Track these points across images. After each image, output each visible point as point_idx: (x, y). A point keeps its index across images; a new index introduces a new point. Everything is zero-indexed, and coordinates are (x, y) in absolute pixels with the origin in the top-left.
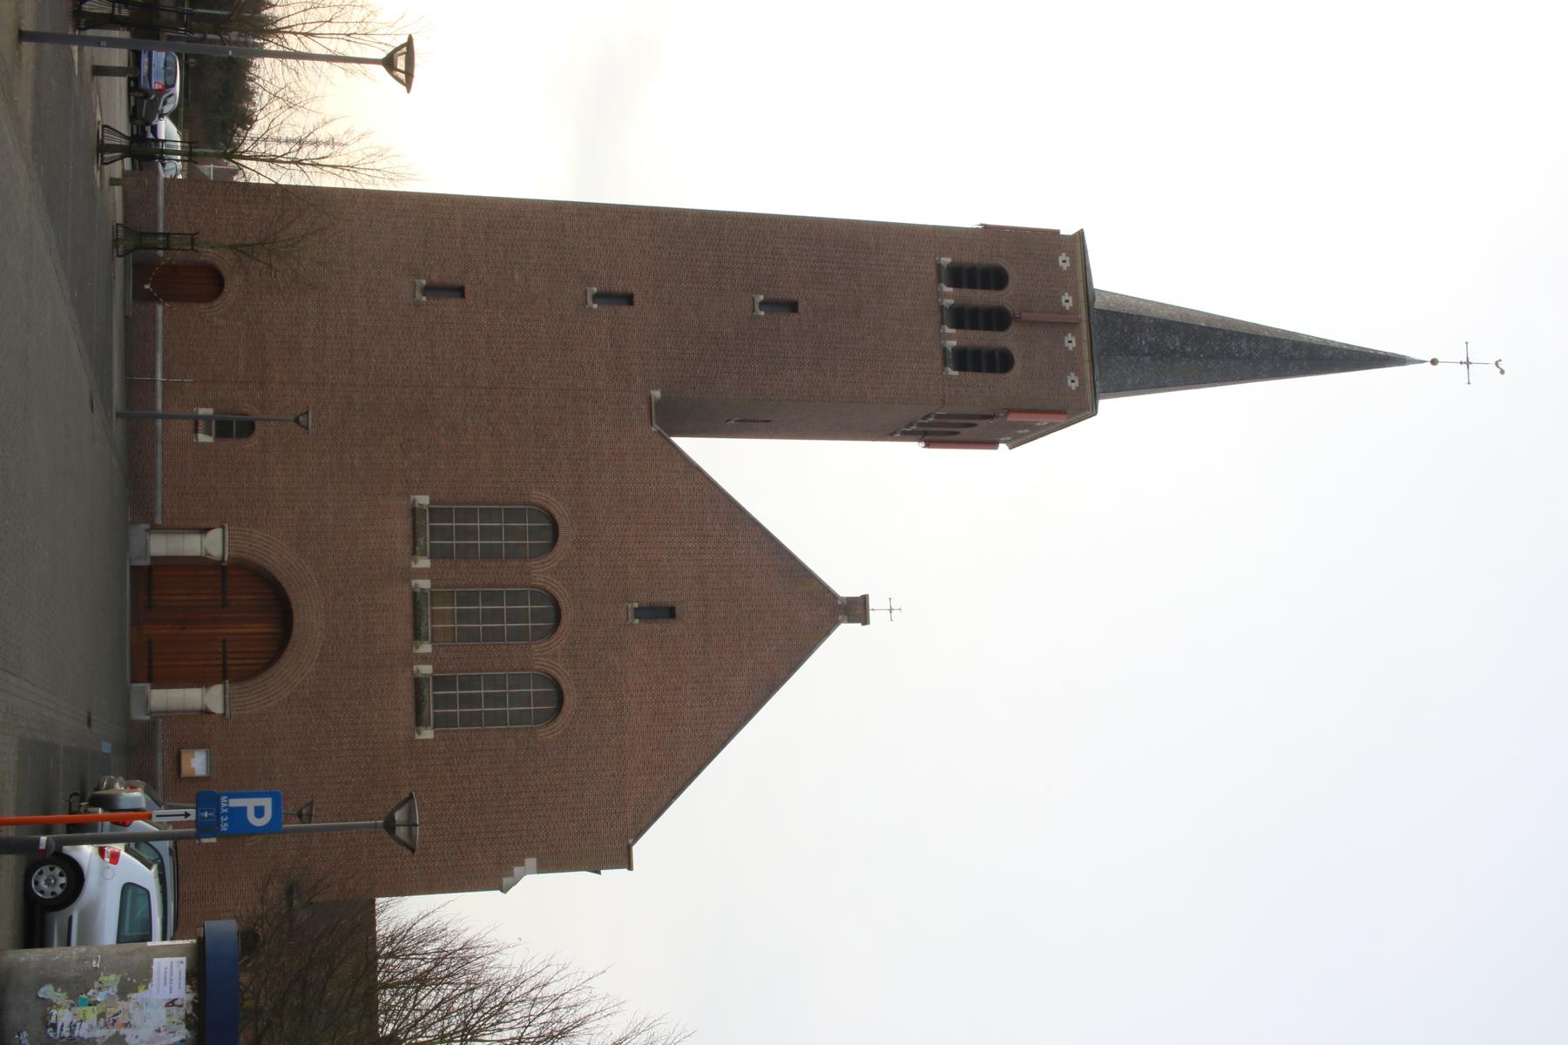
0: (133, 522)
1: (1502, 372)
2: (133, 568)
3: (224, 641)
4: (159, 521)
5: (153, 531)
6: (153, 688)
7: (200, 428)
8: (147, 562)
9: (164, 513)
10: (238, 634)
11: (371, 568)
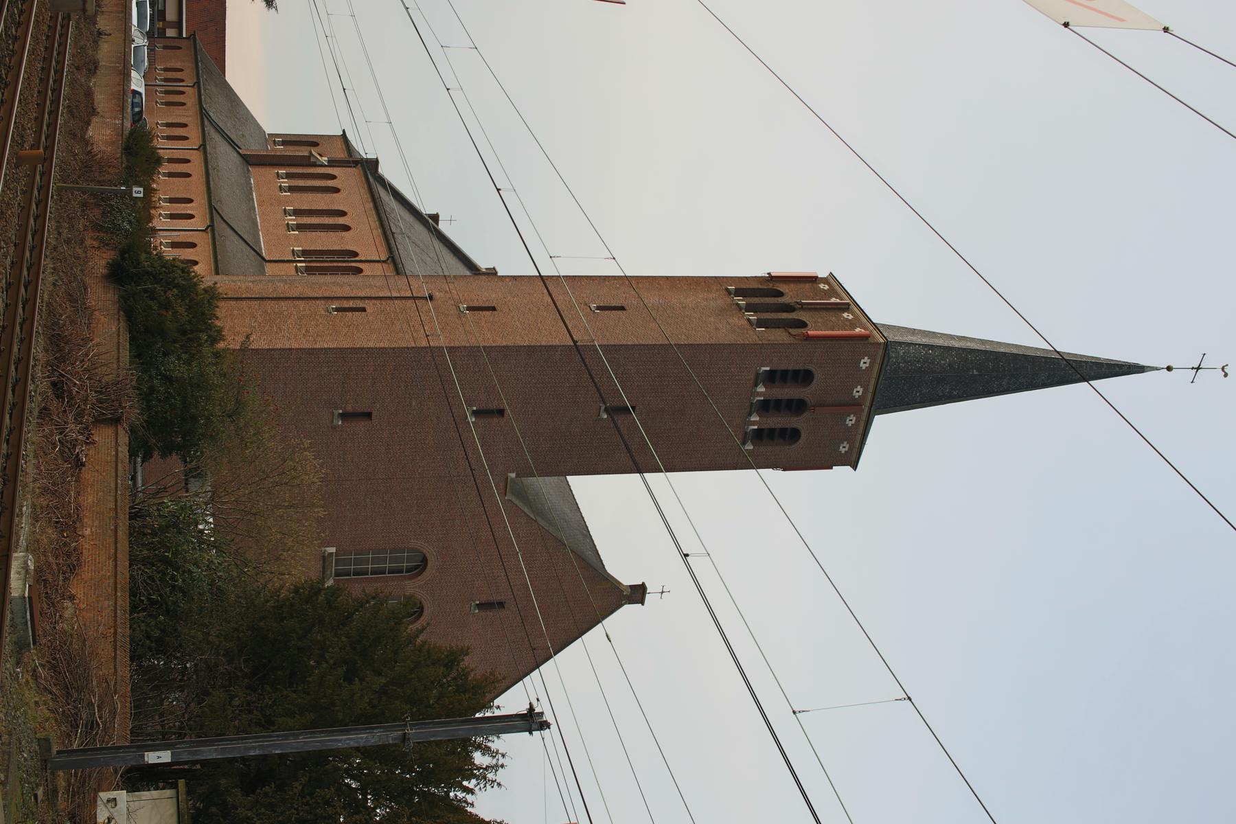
1: (1226, 375)
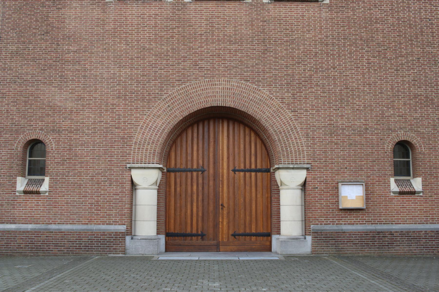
0: (124, 251)
2: (169, 249)
3: (234, 171)
4: (122, 228)
5: (133, 234)
6: (279, 233)
7: (35, 189)
8: (162, 238)
9: (116, 223)
10: (228, 158)
11: (172, 37)
